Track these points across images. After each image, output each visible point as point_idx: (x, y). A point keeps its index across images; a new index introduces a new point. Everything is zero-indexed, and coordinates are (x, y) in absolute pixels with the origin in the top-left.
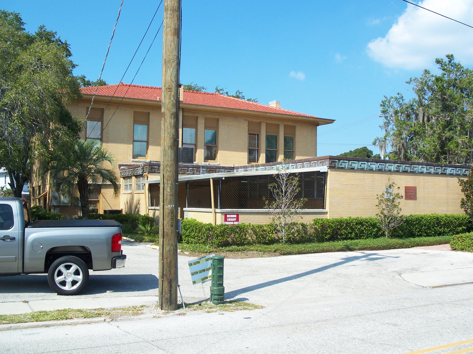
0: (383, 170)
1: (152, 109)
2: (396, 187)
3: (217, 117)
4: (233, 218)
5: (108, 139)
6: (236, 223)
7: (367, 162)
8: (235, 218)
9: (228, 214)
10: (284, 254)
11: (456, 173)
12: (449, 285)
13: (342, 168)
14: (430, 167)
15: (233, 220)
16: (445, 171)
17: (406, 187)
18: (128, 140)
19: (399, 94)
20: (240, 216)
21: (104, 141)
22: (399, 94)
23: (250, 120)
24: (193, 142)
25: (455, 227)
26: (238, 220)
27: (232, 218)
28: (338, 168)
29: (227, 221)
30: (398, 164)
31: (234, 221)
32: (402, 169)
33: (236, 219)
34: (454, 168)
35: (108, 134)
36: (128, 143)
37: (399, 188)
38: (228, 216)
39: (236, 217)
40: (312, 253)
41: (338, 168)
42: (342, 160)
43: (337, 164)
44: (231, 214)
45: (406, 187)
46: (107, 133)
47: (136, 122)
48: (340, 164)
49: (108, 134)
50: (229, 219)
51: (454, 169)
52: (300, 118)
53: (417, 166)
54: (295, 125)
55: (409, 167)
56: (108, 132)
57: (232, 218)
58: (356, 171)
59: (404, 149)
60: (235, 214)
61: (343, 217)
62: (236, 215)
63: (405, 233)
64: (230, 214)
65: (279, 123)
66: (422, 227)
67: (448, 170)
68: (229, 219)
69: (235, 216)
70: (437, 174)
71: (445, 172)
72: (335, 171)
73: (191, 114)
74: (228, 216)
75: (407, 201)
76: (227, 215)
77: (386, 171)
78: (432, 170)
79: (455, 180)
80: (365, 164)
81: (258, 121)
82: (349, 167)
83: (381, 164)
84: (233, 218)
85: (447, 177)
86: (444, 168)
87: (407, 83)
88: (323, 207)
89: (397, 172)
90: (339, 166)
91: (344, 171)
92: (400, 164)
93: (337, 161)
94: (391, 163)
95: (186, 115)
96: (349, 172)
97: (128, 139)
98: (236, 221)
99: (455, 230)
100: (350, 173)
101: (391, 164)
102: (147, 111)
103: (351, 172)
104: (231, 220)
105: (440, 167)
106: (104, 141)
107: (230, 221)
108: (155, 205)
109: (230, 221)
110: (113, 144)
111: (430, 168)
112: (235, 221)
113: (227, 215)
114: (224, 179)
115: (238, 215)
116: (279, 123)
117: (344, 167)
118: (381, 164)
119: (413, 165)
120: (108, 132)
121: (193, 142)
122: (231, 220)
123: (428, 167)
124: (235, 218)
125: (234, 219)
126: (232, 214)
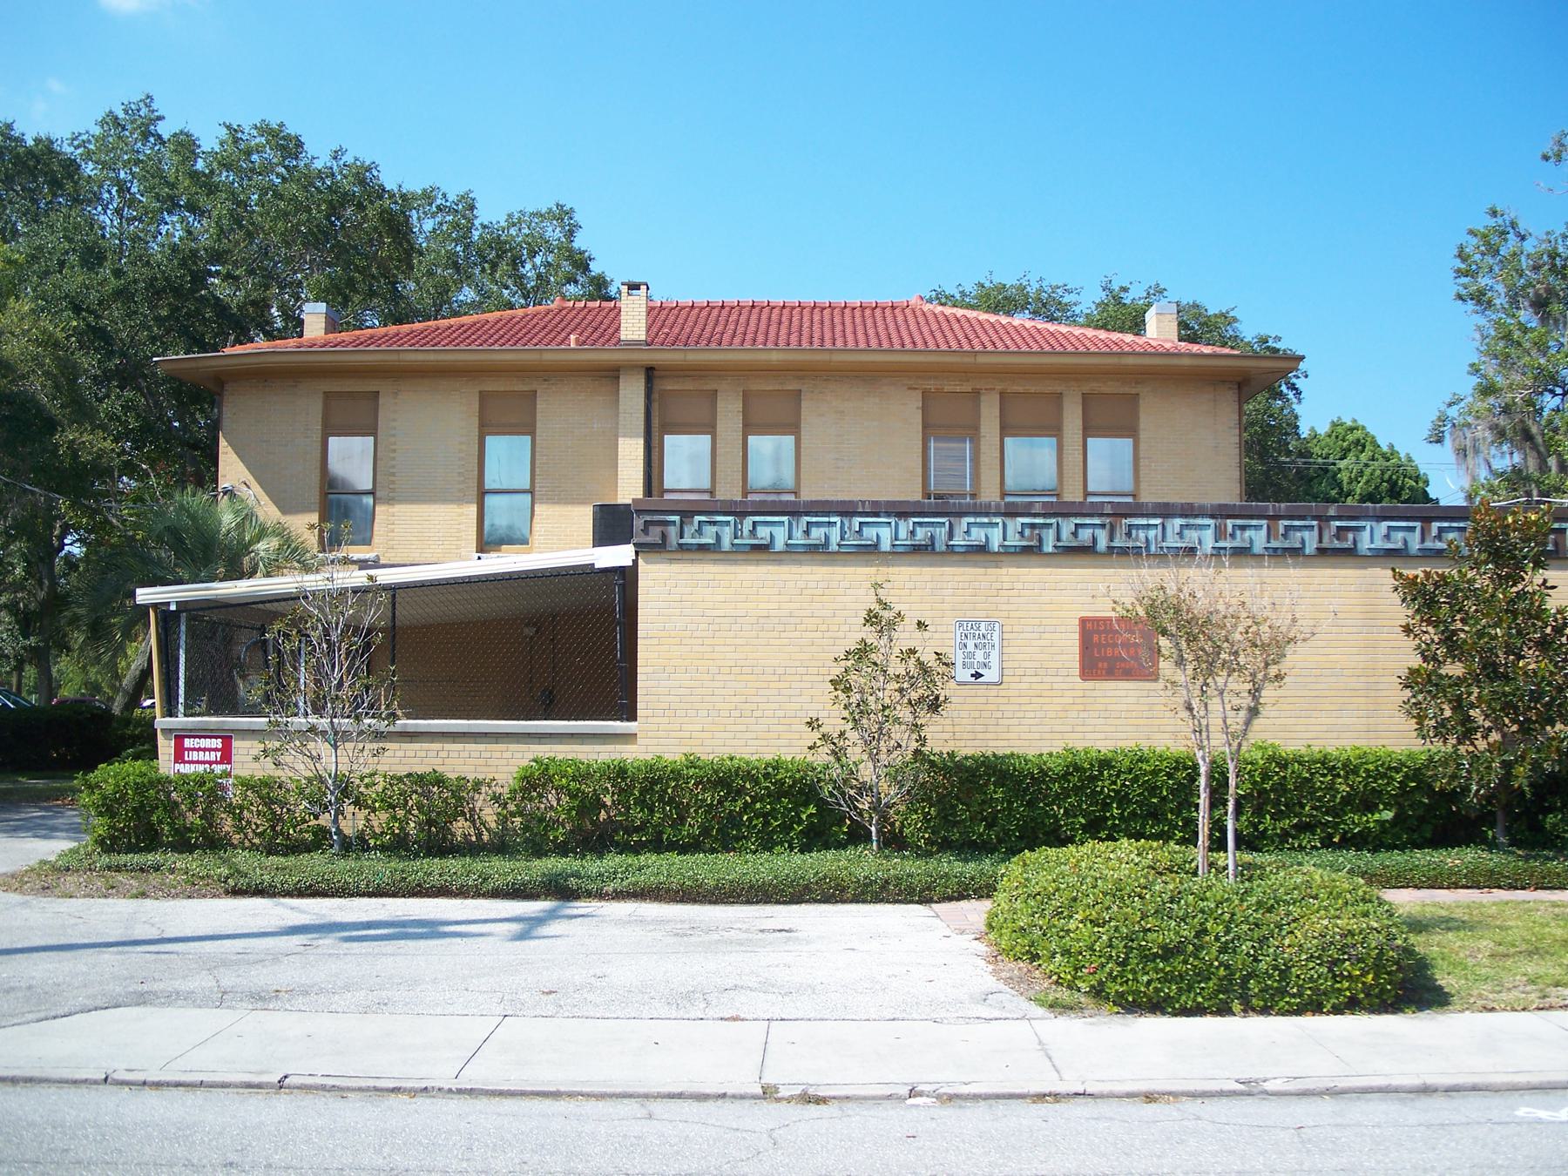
0: (940, 546)
1: (545, 380)
2: (909, 624)
3: (792, 386)
4: (210, 750)
5: (393, 490)
6: (218, 769)
7: (841, 514)
8: (216, 750)
9: (189, 737)
10: (236, 892)
11: (1429, 544)
12: (976, 1097)
13: (702, 548)
14: (1239, 522)
15: (207, 758)
16: (1350, 536)
17: (1084, 621)
18: (460, 490)
19: (1494, 213)
20: (236, 744)
21: (381, 499)
22: (1494, 213)
23: (931, 385)
24: (706, 485)
25: (1336, 812)
26: (226, 756)
27: (204, 750)
28: (682, 548)
29: (185, 762)
30: (1035, 515)
31: (210, 763)
32: (1058, 539)
33: (219, 754)
34: (1411, 524)
35: (393, 474)
36: (460, 500)
37: (920, 624)
38: (188, 743)
39: (220, 746)
40: (363, 895)
41: (682, 548)
42: (700, 513)
43: (673, 532)
44: (200, 737)
45: (1084, 621)
46: (391, 470)
47: (488, 426)
48: (689, 530)
49: (393, 474)
50: (195, 756)
51: (1412, 529)
52: (1131, 361)
53: (1157, 521)
54: (1134, 391)
55: (1103, 526)
56: (393, 467)
57: (204, 750)
58: (783, 557)
59: (1535, 454)
60: (216, 737)
61: (666, 756)
62: (220, 740)
63: (1007, 832)
64: (195, 737)
65: (1058, 388)
66: (1106, 806)
67: (1366, 534)
68: (195, 756)
69: (218, 743)
70: (1296, 552)
71: (1348, 544)
72: (671, 561)
73: (689, 385)
74: (188, 743)
75: (1089, 684)
76: (186, 740)
77: (957, 549)
78: (1258, 538)
79: (1382, 576)
80: (1412, 529)
81: (967, 387)
82: (736, 541)
83: (926, 520)
84: (210, 750)
85: (1365, 568)
86: (1338, 523)
87: (1546, 158)
88: (632, 716)
89: (1031, 551)
90: (687, 540)
91: (715, 561)
92: (1044, 515)
93: (676, 518)
94: (987, 514)
95: (669, 388)
96: (747, 562)
97: (461, 486)
98: (221, 762)
99: (1338, 823)
100: (751, 568)
101: (986, 520)
102: (526, 388)
103: (758, 562)
104: (202, 756)
105: (1314, 518)
106: (381, 499)
107: (198, 762)
108: (181, 708)
109: (198, 762)
110: (408, 506)
111: (1243, 528)
112: (216, 762)
113: (186, 740)
114: (173, 607)
115: (227, 741)
116: (1058, 388)
117: (711, 541)
118: (926, 520)
119: (1126, 516)
120: (393, 467)
121: (706, 485)
122: (202, 756)
123: (1230, 523)
124: (190, 749)
125: (213, 753)
126: (205, 737)
